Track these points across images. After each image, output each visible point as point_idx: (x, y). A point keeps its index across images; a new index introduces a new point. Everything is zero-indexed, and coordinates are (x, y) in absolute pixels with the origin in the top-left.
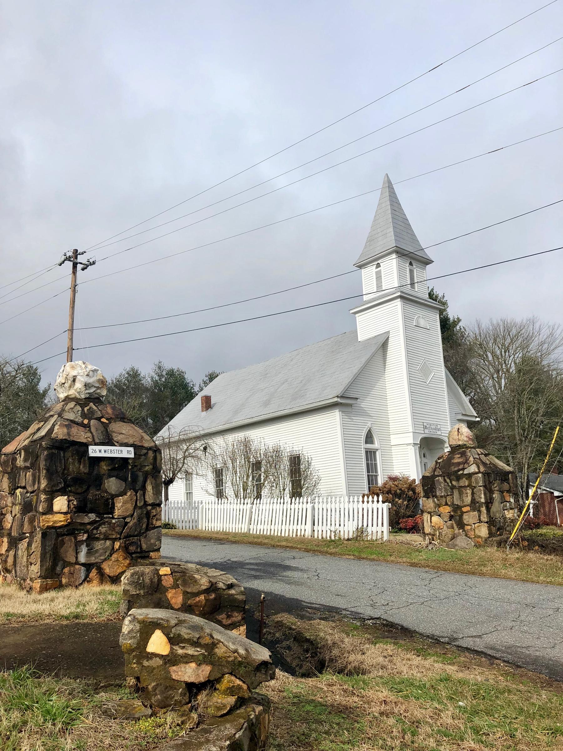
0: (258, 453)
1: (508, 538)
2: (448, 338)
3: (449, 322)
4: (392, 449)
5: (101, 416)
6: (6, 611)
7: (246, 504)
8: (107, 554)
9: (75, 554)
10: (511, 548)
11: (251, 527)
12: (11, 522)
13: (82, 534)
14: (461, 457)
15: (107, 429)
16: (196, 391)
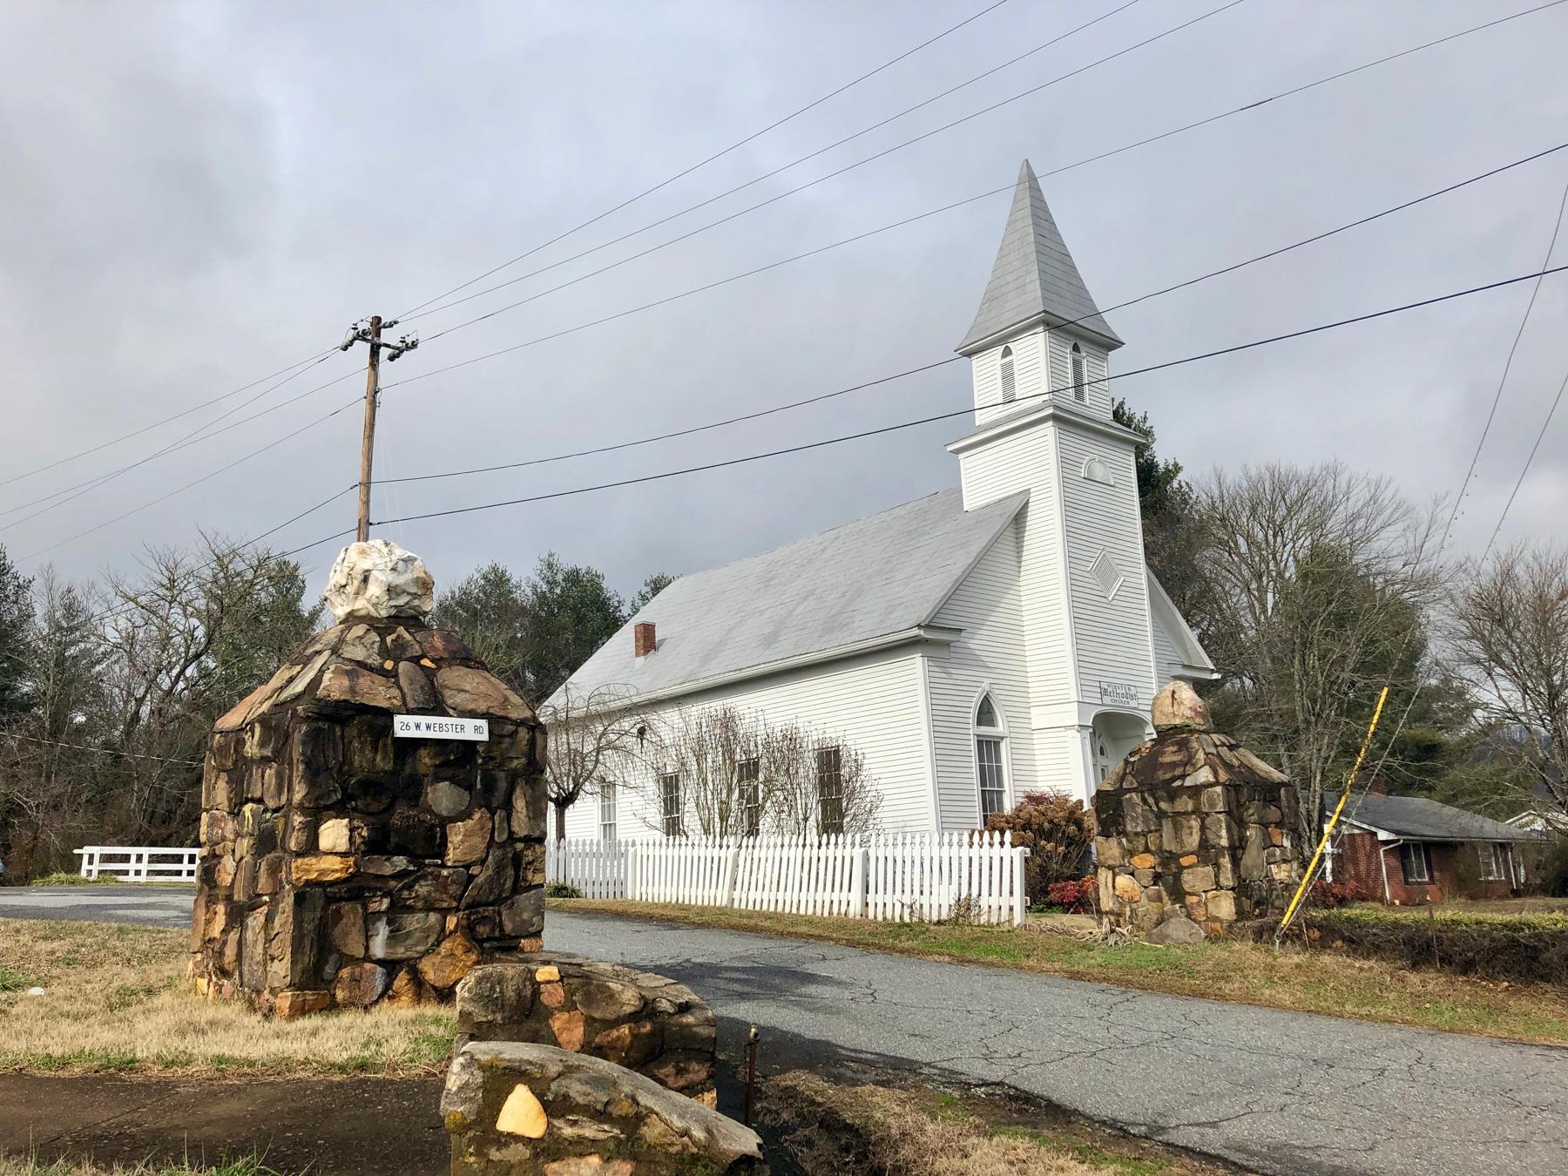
0: (752, 744)
1: (1278, 922)
2: (1153, 507)
3: (1157, 472)
4: (1034, 737)
5: (420, 653)
6: (217, 1054)
7: (725, 848)
8: (431, 940)
9: (363, 940)
10: (1283, 943)
11: (736, 895)
12: (232, 872)
13: (378, 899)
14: (1179, 750)
15: (432, 682)
16: (626, 615)
